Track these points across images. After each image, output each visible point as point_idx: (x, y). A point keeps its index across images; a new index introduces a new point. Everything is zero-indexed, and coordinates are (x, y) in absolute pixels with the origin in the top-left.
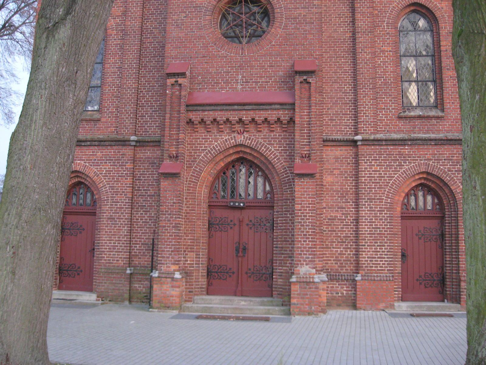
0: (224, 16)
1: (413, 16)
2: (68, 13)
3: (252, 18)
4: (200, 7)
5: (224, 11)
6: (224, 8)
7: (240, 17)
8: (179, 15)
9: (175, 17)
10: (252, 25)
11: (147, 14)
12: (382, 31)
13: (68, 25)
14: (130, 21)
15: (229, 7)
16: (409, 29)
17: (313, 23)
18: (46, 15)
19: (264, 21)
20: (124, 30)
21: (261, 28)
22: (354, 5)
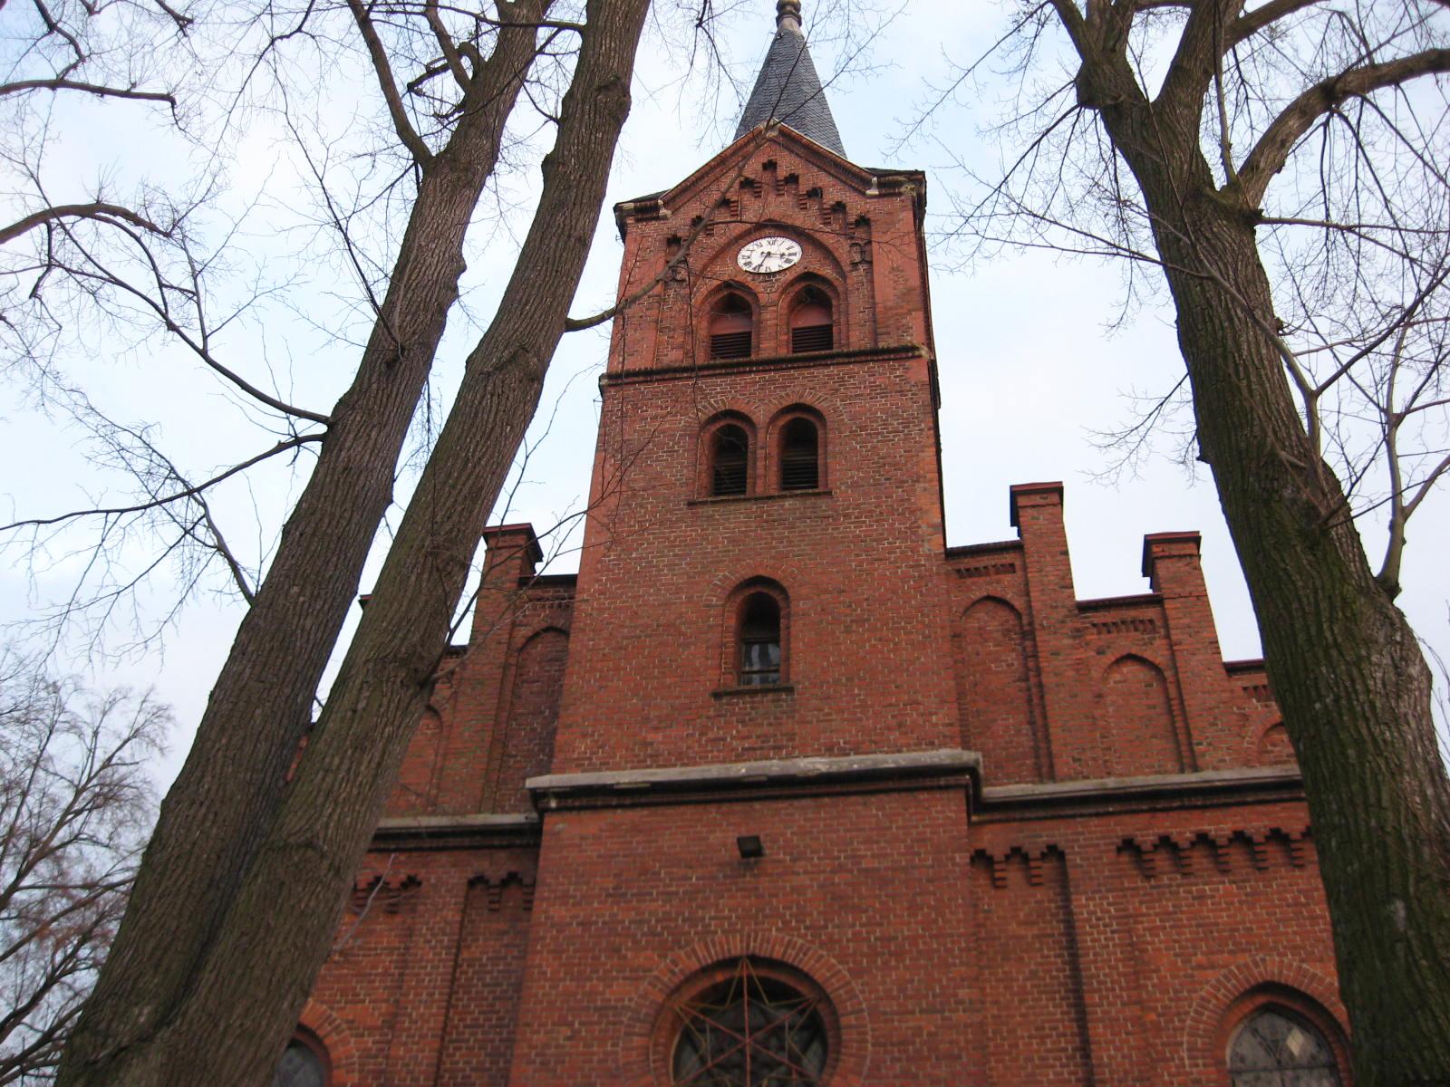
0: (688, 1039)
1: (1265, 1023)
2: (162, 1021)
3: (774, 1042)
4: (615, 1008)
5: (687, 1021)
6: (687, 1014)
7: (736, 1041)
8: (551, 1032)
9: (538, 1038)
10: (771, 1065)
11: (456, 1027)
12: (1178, 1074)
13: (156, 1057)
14: (405, 1044)
15: (703, 1012)
16: (1260, 1065)
17: (959, 1057)
18: (98, 1024)
19: (810, 1053)
20: (383, 1072)
21: (801, 1074)
22: (1082, 998)
